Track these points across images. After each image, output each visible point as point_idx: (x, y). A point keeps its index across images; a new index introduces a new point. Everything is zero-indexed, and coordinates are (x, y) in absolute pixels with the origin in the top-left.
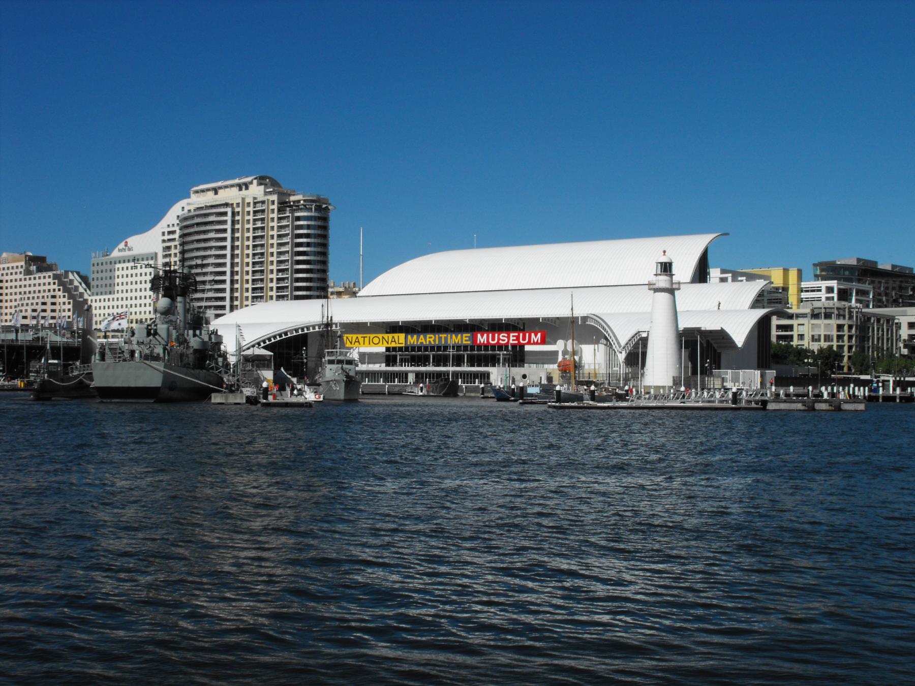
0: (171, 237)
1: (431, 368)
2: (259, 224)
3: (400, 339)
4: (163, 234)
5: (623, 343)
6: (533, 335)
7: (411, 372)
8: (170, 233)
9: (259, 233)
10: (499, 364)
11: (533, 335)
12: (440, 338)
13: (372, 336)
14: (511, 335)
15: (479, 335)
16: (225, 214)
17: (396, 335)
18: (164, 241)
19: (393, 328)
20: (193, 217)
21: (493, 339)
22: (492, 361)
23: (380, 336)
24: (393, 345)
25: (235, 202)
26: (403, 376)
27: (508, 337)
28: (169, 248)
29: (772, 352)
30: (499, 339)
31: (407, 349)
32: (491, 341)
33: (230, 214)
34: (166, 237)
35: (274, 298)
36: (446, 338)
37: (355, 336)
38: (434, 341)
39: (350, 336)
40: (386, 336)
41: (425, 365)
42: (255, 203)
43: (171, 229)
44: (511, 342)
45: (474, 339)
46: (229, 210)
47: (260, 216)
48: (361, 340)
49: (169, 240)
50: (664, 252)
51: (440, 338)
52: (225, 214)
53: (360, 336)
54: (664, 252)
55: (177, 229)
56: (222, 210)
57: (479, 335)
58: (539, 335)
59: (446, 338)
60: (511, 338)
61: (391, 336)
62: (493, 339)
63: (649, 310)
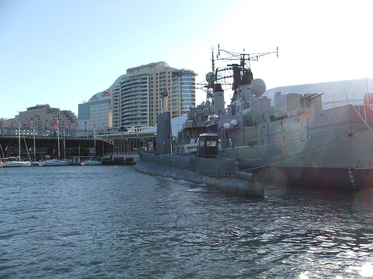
8: (116, 90)
33: (148, 79)
34: (115, 92)
43: (117, 88)
46: (148, 77)
52: (146, 78)
55: (120, 88)
56: (144, 77)
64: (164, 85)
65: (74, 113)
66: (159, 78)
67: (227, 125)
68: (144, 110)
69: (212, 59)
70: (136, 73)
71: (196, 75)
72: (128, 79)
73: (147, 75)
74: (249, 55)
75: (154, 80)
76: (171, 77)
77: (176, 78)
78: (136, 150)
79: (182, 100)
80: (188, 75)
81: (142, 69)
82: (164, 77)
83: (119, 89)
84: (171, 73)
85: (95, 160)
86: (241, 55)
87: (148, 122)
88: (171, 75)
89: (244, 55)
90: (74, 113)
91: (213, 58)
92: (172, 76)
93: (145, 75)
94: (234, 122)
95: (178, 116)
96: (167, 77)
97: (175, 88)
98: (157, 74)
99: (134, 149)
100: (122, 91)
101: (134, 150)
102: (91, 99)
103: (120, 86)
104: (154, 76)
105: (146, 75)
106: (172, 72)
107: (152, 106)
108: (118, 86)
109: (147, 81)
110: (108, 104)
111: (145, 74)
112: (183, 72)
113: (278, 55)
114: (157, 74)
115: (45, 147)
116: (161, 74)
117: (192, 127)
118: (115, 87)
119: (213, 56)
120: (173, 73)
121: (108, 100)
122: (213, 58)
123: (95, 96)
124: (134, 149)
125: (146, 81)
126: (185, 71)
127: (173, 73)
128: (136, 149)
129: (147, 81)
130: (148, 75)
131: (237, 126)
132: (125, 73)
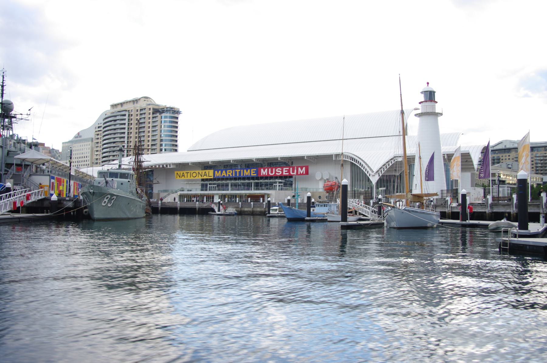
0: (99, 129)
1: (230, 192)
3: (210, 173)
5: (375, 170)
6: (245, 171)
7: (217, 194)
8: (99, 127)
10: (532, 187)
12: (236, 172)
13: (192, 172)
14: (284, 169)
15: (262, 170)
16: (125, 115)
17: (207, 171)
19: (206, 166)
21: (272, 172)
22: (270, 186)
23: (197, 172)
24: (205, 177)
25: (130, 110)
26: (210, 198)
27: (282, 171)
28: (98, 135)
29: (374, 180)
30: (276, 172)
31: (214, 179)
32: (270, 174)
33: (127, 115)
34: (97, 130)
36: (240, 173)
37: (182, 172)
38: (232, 174)
39: (179, 172)
40: (200, 172)
41: (248, 189)
43: (99, 125)
44: (284, 174)
45: (258, 172)
46: (127, 113)
48: (186, 175)
50: (428, 83)
51: (236, 172)
52: (125, 115)
53: (185, 172)
54: (428, 83)
57: (262, 170)
58: (304, 169)
59: (240, 173)
60: (284, 171)
61: (204, 171)
62: (272, 172)
65: (433, 180)
66: (151, 118)
70: (119, 108)
72: (109, 115)
76: (151, 114)
79: (161, 140)
81: (125, 104)
84: (151, 109)
85: (142, 197)
88: (151, 111)
90: (433, 180)
91: (3, 83)
92: (153, 113)
97: (156, 117)
100: (104, 128)
102: (76, 137)
105: (126, 111)
110: (90, 143)
114: (137, 110)
115: (282, 168)
116: (141, 110)
120: (153, 109)
123: (79, 133)
126: (167, 108)
127: (153, 109)
129: (126, 117)
132: (109, 108)
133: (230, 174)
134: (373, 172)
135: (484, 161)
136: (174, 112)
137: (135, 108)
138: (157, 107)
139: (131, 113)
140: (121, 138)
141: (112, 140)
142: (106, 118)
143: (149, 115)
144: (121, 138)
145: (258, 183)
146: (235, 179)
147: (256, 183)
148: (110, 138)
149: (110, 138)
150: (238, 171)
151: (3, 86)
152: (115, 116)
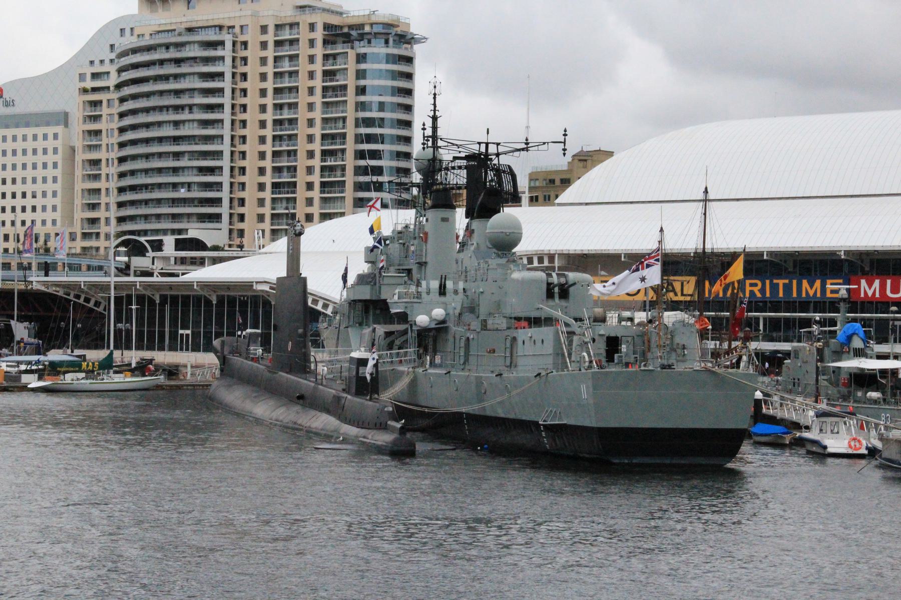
2: (286, 66)
4: (82, 77)
6: (805, 283)
8: (95, 76)
9: (286, 83)
11: (805, 283)
18: (85, 91)
20: (149, 49)
28: (96, 104)
33: (229, 45)
34: (89, 84)
35: (316, 217)
36: (788, 288)
38: (762, 291)
42: (278, 27)
43: (98, 69)
46: (228, 39)
47: (286, 51)
49: (95, 90)
50: (543, 341)
51: (775, 288)
54: (543, 341)
55: (113, 69)
56: (212, 36)
59: (788, 288)
63: (488, 327)
64: (290, 76)
67: (422, 320)
68: (211, 170)
69: (432, 114)
71: (418, 41)
72: (147, 41)
73: (225, 31)
74: (498, 144)
75: (253, 53)
77: (339, 49)
78: (187, 335)
80: (387, 42)
82: (290, 89)
83: (108, 73)
86: (479, 143)
87: (225, 218)
88: (319, 35)
89: (487, 144)
91: (435, 111)
92: (326, 42)
93: (217, 29)
94: (438, 313)
95: (342, 214)
96: (303, 43)
97: (334, 56)
98: (264, 29)
99: (181, 332)
101: (182, 335)
103: (112, 61)
104: (252, 37)
105: (221, 27)
106: (325, 24)
107: (240, 152)
108: (102, 62)
109: (226, 52)
111: (215, 26)
112: (367, 29)
113: (564, 150)
114: (264, 29)
116: (278, 27)
117: (368, 297)
118: (92, 62)
119: (435, 105)
120: (327, 27)
121: (58, 114)
122: (435, 111)
124: (181, 332)
125: (219, 53)
128: (189, 332)
129: (226, 52)
130: (229, 27)
131: (443, 322)
133: (756, 290)
134: (64, 119)
135: (849, 397)
136: (398, 37)
137: (255, 15)
138: (334, 20)
139: (242, 38)
140: (205, 123)
141: (169, 131)
142: (135, 51)
143: (311, 53)
144: (205, 123)
145: (778, 320)
146: (776, 306)
147: (771, 319)
148: (159, 124)
149: (159, 124)
150: (781, 282)
151: (435, 119)
152: (179, 46)
